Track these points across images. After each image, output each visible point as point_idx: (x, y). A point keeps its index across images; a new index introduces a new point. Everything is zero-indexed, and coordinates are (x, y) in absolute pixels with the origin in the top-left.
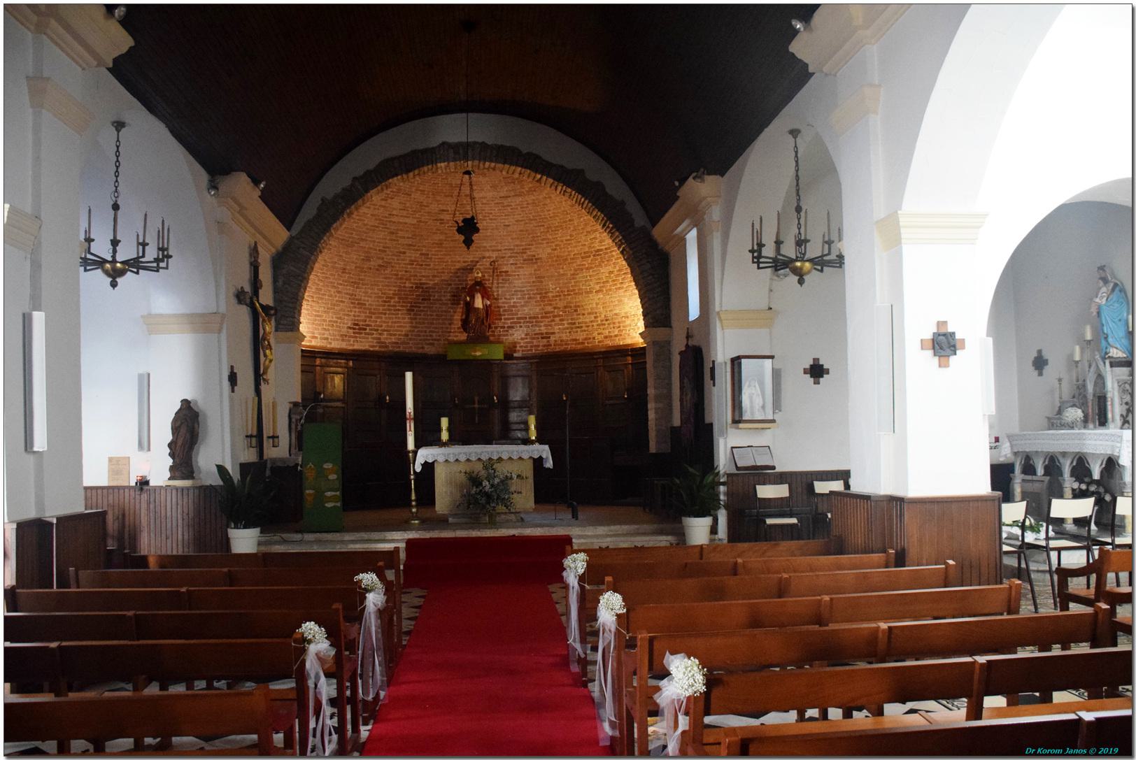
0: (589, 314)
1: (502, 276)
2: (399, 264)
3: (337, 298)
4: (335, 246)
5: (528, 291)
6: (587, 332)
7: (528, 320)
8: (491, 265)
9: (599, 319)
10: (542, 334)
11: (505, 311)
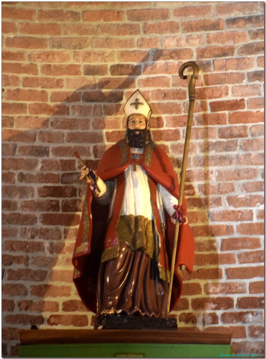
1: (219, 120)
11: (229, 244)
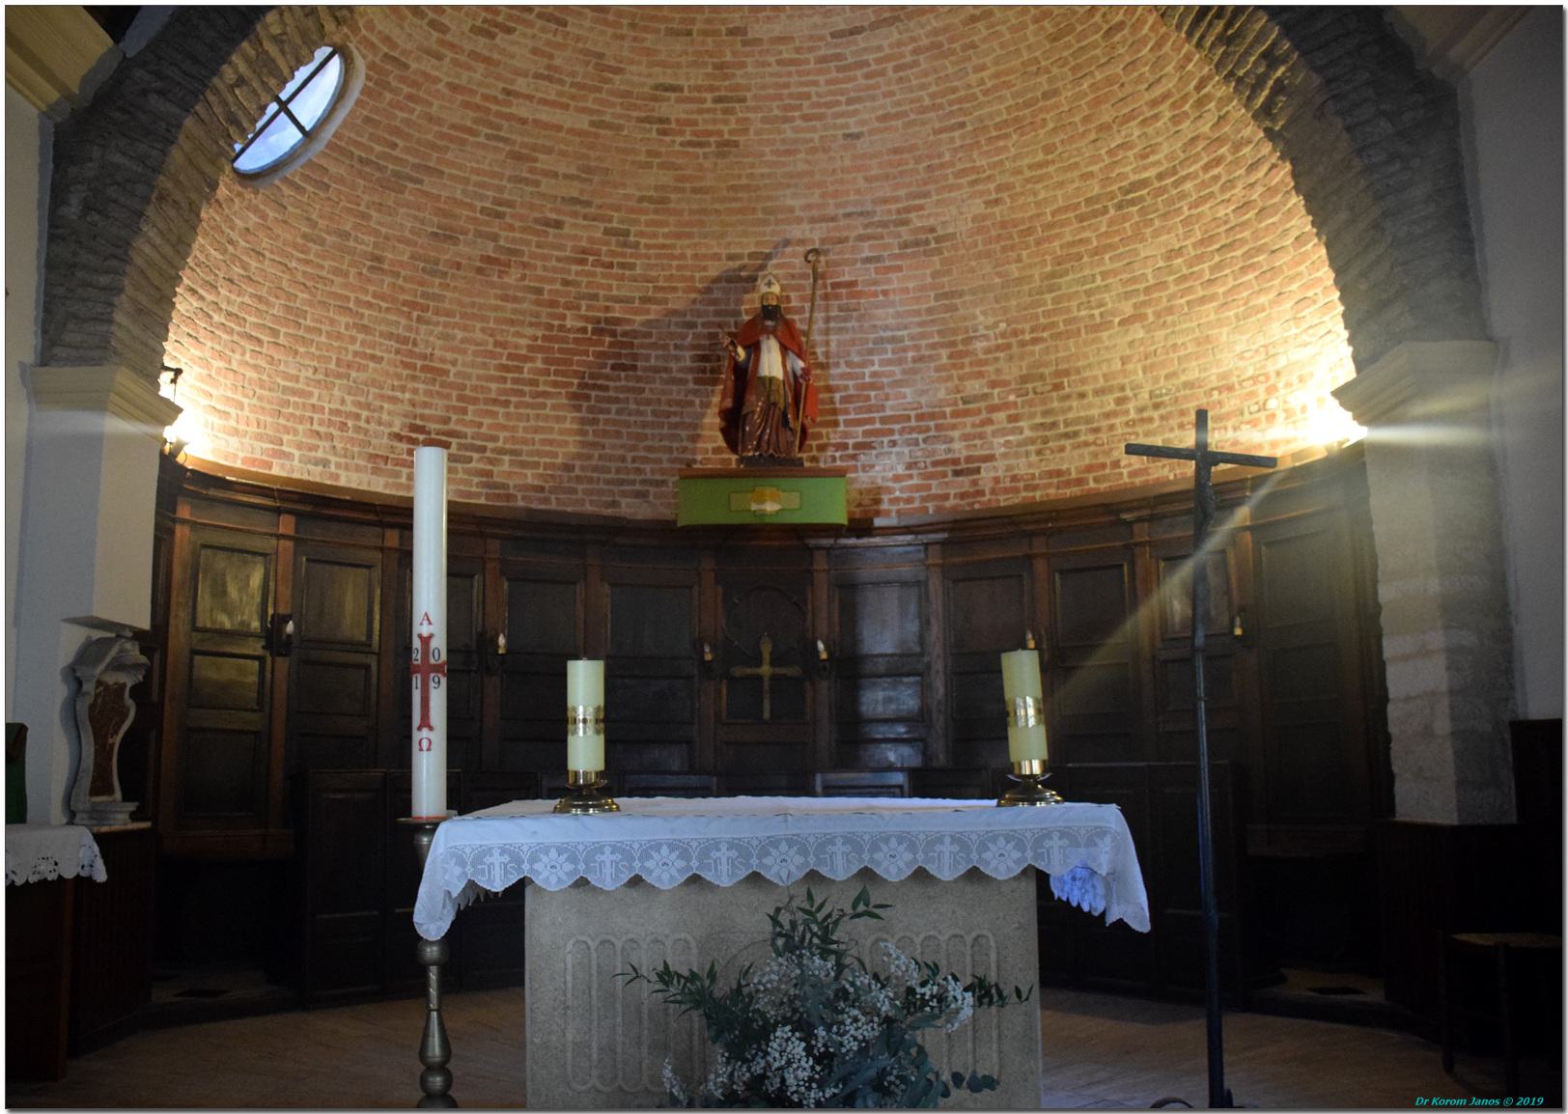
0: (1097, 393)
1: (837, 297)
2: (545, 258)
3: (357, 347)
4: (341, 180)
5: (912, 338)
6: (1092, 448)
7: (913, 423)
9: (1131, 406)
10: (956, 461)
11: (846, 400)
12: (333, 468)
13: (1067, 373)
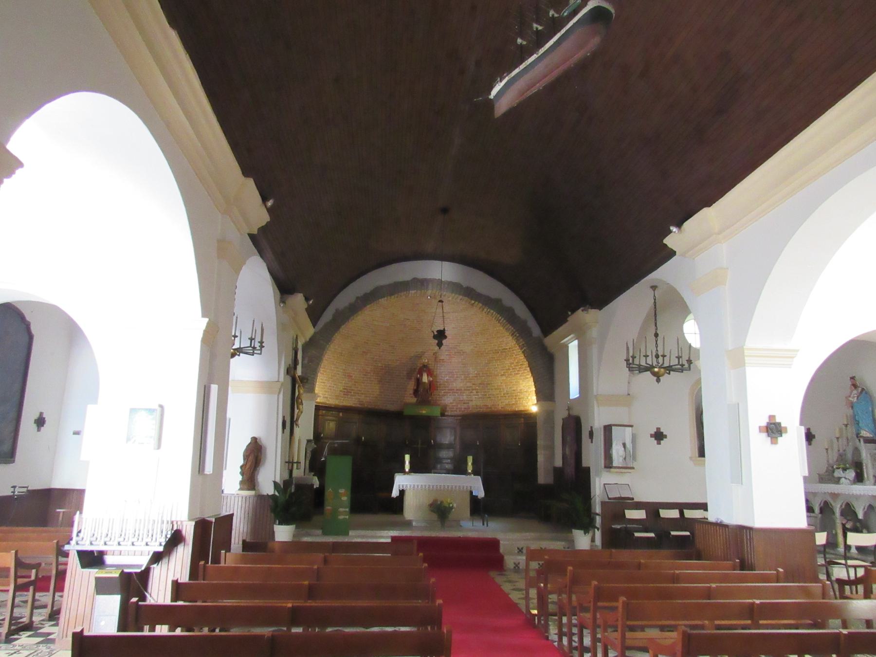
0: (496, 389)
8: (434, 354)
12: (328, 399)
13: (489, 384)
